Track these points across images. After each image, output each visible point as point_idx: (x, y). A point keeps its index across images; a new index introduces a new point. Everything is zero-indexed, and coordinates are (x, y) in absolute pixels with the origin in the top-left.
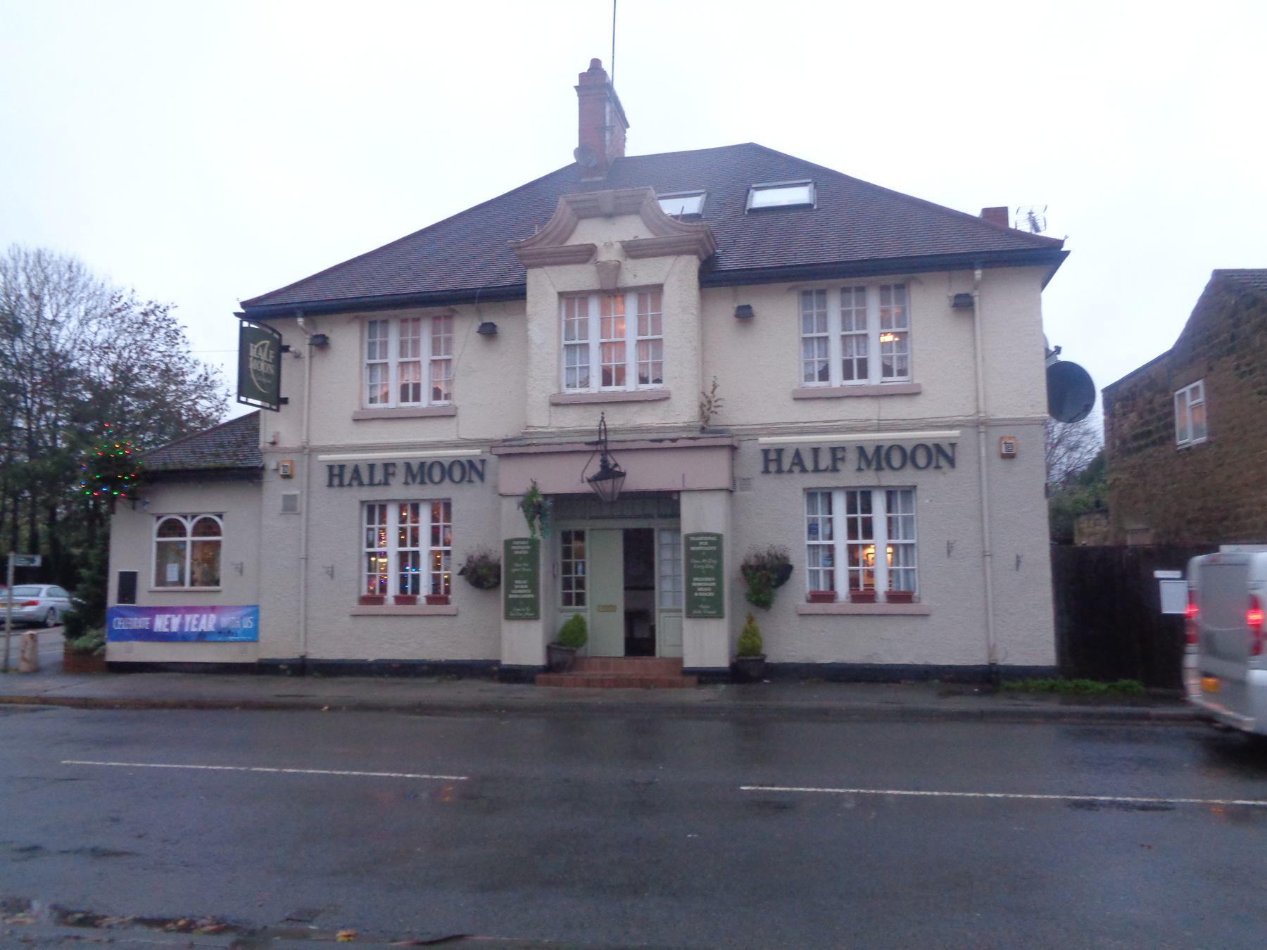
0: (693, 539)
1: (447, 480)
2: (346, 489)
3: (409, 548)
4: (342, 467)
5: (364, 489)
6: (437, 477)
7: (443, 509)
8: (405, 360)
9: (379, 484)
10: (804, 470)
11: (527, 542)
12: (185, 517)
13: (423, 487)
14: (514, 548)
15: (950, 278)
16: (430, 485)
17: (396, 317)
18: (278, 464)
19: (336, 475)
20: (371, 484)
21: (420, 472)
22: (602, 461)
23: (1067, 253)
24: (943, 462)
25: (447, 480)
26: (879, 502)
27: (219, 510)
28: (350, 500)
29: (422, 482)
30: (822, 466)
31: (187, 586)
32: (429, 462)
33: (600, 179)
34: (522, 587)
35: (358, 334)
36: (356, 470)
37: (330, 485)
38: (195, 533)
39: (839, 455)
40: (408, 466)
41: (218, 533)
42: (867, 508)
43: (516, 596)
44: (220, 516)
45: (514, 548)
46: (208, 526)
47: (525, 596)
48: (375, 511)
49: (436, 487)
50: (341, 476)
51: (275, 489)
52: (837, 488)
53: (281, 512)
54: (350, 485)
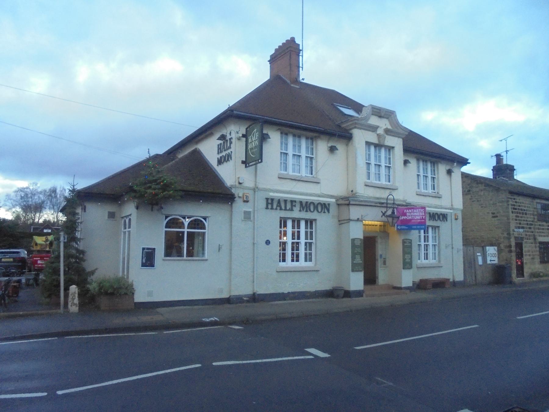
1: (316, 211)
3: (296, 241)
4: (272, 200)
5: (282, 211)
6: (312, 210)
7: (310, 223)
8: (295, 153)
9: (289, 210)
11: (359, 240)
13: (307, 213)
14: (355, 242)
17: (292, 133)
18: (244, 194)
19: (270, 203)
20: (286, 209)
21: (306, 206)
22: (392, 210)
23: (469, 163)
24: (326, 211)
25: (316, 211)
26: (303, 224)
28: (276, 215)
29: (307, 211)
30: (288, 208)
31: (185, 257)
32: (310, 201)
34: (358, 258)
35: (280, 137)
36: (279, 201)
37: (267, 208)
40: (301, 203)
41: (204, 228)
42: (299, 227)
43: (356, 262)
45: (355, 242)
46: (197, 224)
47: (359, 262)
48: (283, 222)
49: (318, 213)
50: (272, 204)
51: (239, 207)
52: (303, 219)
53: (243, 219)
54: (276, 209)
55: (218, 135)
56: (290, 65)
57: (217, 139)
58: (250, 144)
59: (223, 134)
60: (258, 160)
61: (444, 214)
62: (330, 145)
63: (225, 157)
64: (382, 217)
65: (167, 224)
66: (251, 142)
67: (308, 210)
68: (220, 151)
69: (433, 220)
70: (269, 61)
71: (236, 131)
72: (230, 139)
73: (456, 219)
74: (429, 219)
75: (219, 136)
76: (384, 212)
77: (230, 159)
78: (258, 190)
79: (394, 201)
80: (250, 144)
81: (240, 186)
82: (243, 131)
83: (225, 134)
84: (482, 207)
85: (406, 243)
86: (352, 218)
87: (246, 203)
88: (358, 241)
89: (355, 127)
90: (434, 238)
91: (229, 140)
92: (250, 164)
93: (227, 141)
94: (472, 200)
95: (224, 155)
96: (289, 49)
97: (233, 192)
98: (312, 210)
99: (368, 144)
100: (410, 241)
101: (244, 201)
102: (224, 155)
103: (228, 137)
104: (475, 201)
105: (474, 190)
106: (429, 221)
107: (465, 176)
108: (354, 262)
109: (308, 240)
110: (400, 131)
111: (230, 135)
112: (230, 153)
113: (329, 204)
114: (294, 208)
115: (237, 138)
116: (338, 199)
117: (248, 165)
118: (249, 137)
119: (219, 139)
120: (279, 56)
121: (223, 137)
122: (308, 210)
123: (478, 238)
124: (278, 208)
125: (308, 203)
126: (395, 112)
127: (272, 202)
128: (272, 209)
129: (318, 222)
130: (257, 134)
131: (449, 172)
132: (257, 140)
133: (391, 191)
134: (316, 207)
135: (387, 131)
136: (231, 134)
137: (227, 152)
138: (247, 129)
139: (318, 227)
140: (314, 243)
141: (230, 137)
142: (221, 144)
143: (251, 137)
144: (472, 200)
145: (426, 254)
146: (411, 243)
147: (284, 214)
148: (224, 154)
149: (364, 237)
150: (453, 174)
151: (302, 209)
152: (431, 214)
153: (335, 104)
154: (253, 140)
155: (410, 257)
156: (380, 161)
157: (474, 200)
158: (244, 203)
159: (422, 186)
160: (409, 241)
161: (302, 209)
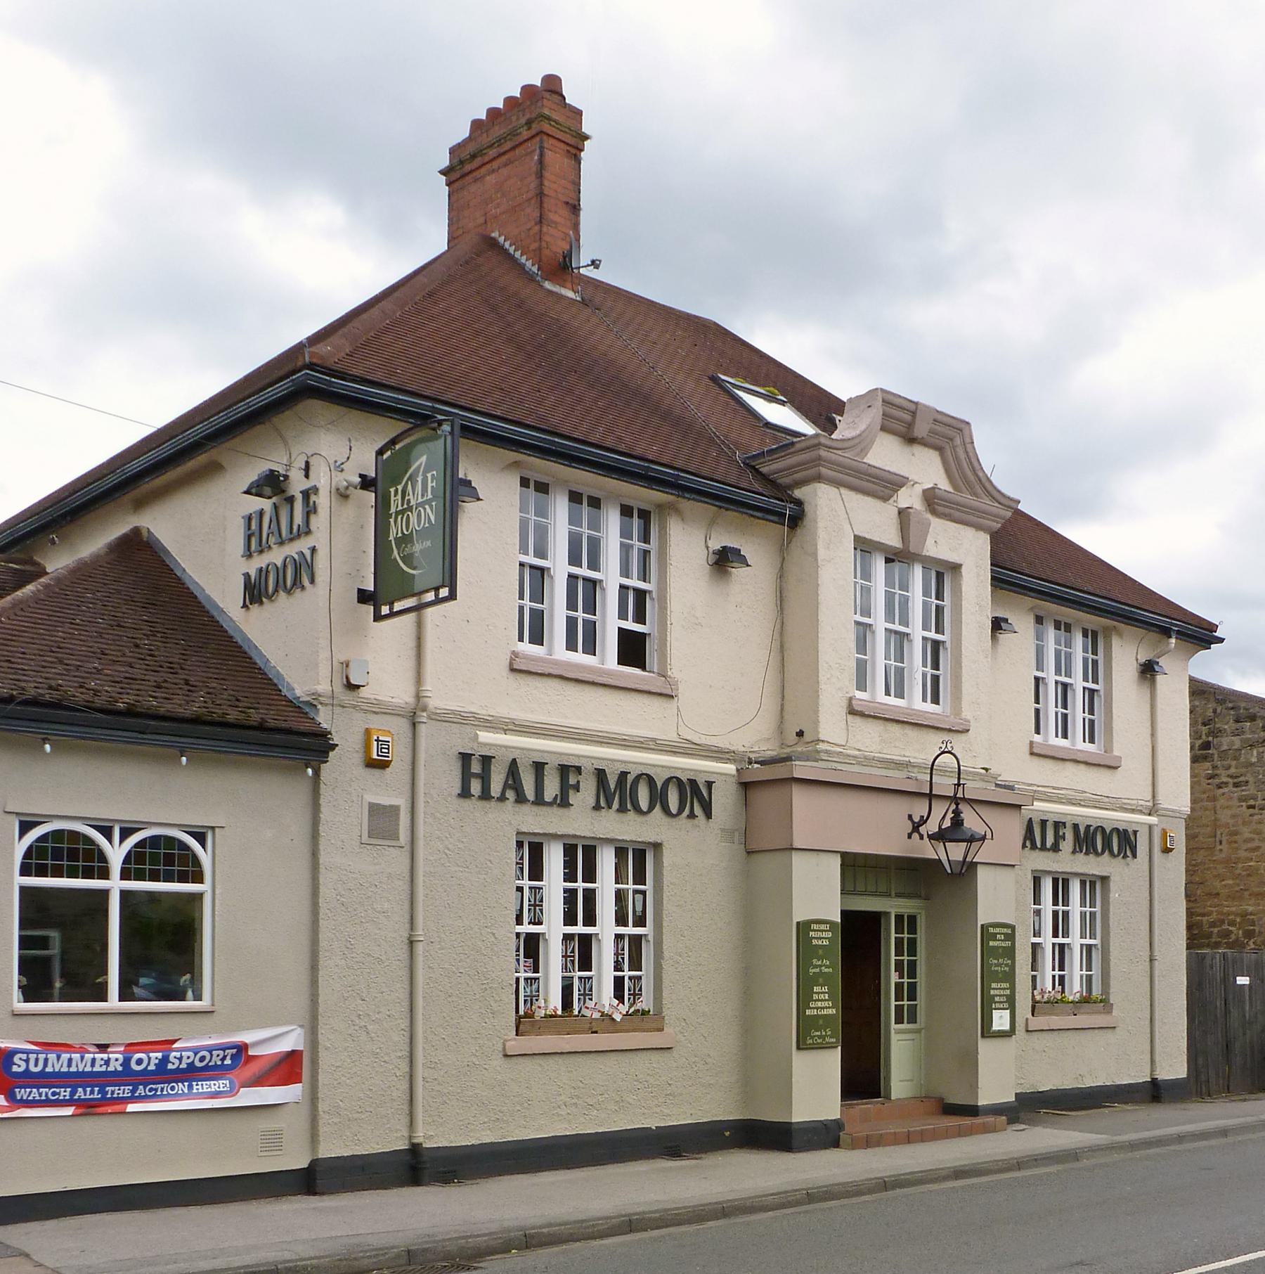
0: (991, 930)
2: (493, 803)
3: (580, 929)
4: (486, 760)
5: (526, 808)
6: (644, 804)
10: (521, 799)
12: (107, 832)
15: (683, 520)
16: (632, 815)
20: (539, 801)
23: (1221, 640)
24: (698, 810)
26: (606, 862)
27: (198, 819)
29: (622, 809)
30: (548, 796)
31: (113, 1001)
33: (570, 294)
34: (822, 996)
37: (465, 793)
38: (125, 875)
39: (572, 781)
44: (200, 838)
47: (825, 1012)
48: (1061, 886)
50: (485, 778)
53: (365, 838)
54: (502, 798)
55: (252, 472)
56: (541, 195)
57: (246, 492)
58: (396, 522)
59: (272, 471)
60: (437, 589)
61: (1125, 831)
62: (715, 545)
63: (281, 571)
64: (910, 836)
65: (28, 854)
66: (402, 512)
67: (629, 806)
68: (254, 541)
69: (1087, 853)
70: (443, 172)
71: (331, 462)
72: (306, 494)
73: (1167, 851)
74: (1071, 850)
75: (256, 478)
76: (916, 819)
77: (306, 582)
78: (429, 718)
79: (959, 779)
80: (396, 522)
81: (347, 697)
82: (364, 459)
83: (282, 472)
84: (1253, 807)
85: (995, 940)
86: (797, 845)
87: (377, 772)
88: (822, 931)
89: (818, 478)
90: (1088, 924)
91: (299, 497)
92: (398, 606)
93: (291, 500)
94: (1217, 781)
95: (279, 563)
96: (535, 127)
97: (324, 725)
98: (644, 804)
99: (864, 547)
100: (1009, 931)
101: (372, 764)
102: (279, 563)
103: (297, 484)
104: (1226, 783)
105: (1225, 742)
106: (1072, 857)
107: (1199, 690)
108: (808, 1012)
109: (626, 925)
110: (985, 503)
111: (307, 476)
112: (308, 553)
113: (709, 785)
114: (573, 798)
115: (338, 489)
116: (744, 760)
117: (385, 610)
118: (392, 490)
119: (255, 490)
120: (493, 153)
121: (272, 484)
122: (629, 806)
123: (1232, 923)
124: (510, 795)
125: (630, 778)
126: (968, 423)
127: (483, 769)
128: (485, 795)
129: (668, 858)
130: (429, 475)
131: (1148, 670)
132: (429, 502)
133: (946, 737)
134: (658, 797)
135: (932, 499)
136: (311, 473)
137: (292, 550)
138: (380, 452)
139: (668, 877)
140: (651, 938)
141: (306, 485)
142: (261, 513)
143: (400, 488)
144: (1217, 781)
145: (1084, 977)
146: (1011, 937)
147: (535, 821)
148: (276, 556)
149: (844, 913)
150: (1159, 678)
151: (603, 803)
152: (1082, 830)
153: (723, 377)
154: (413, 503)
155: (1008, 992)
156: (905, 621)
157: (1225, 779)
158: (367, 769)
159: (1050, 723)
160: (1005, 930)
161: (603, 803)
